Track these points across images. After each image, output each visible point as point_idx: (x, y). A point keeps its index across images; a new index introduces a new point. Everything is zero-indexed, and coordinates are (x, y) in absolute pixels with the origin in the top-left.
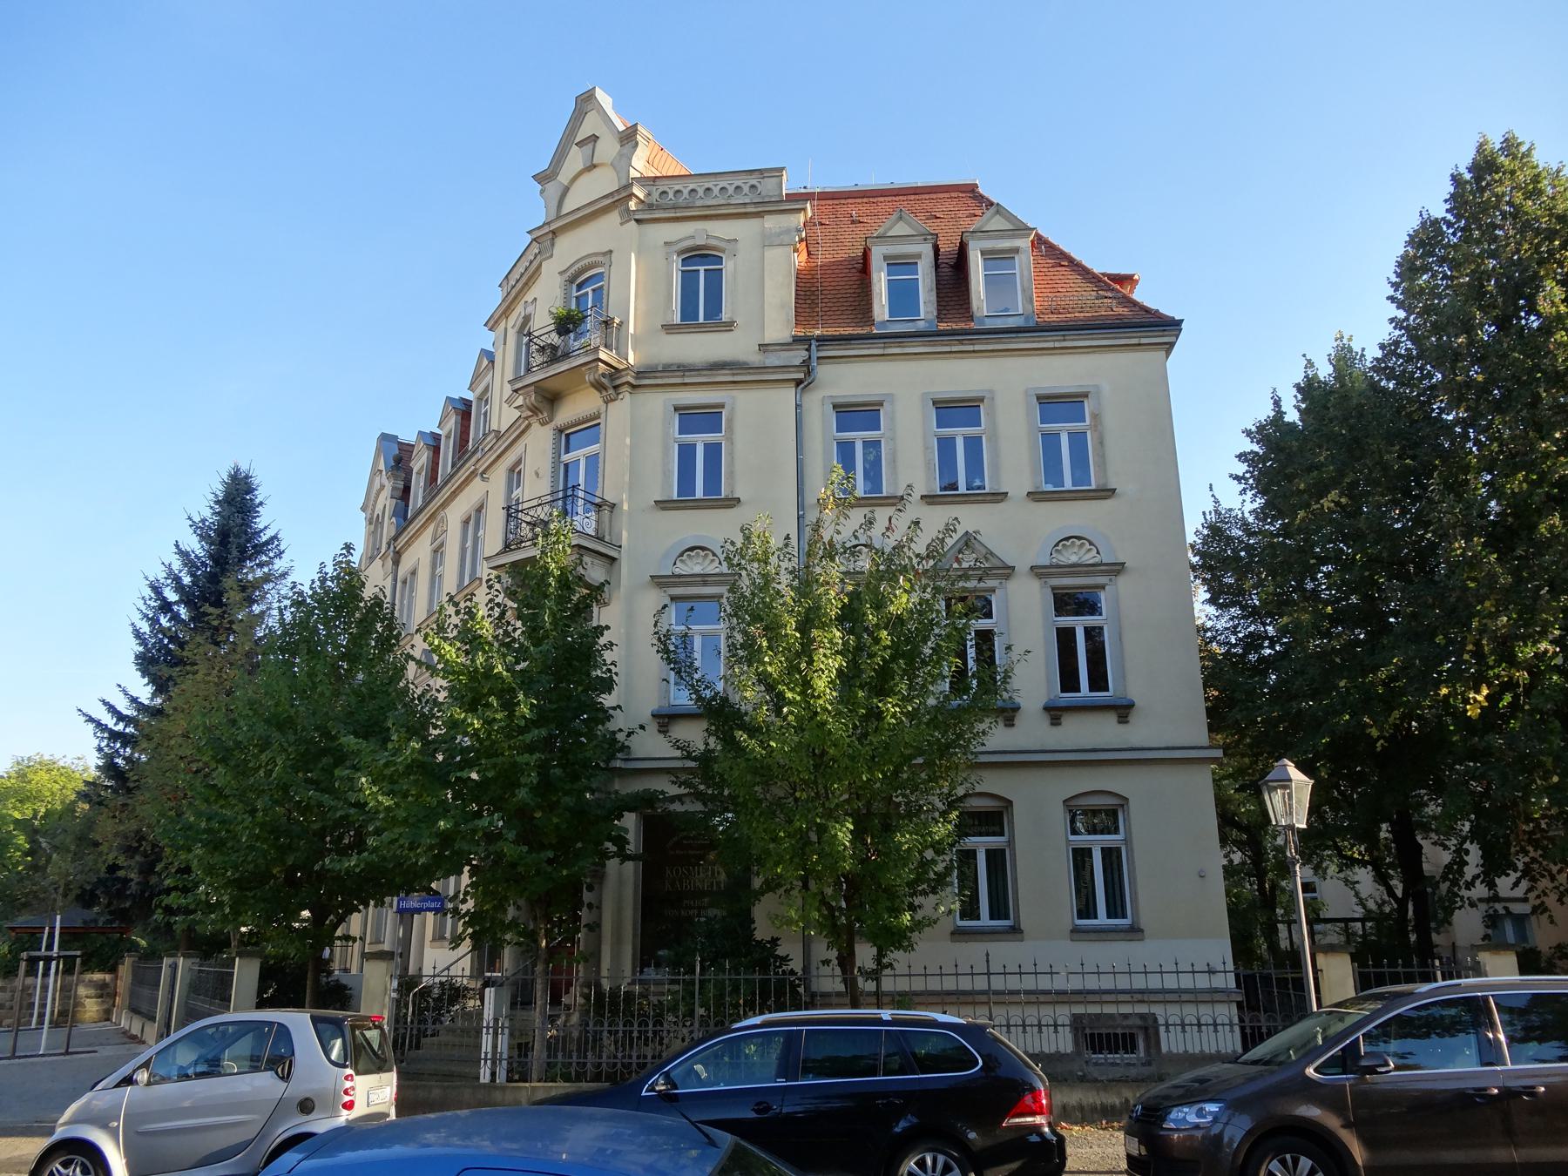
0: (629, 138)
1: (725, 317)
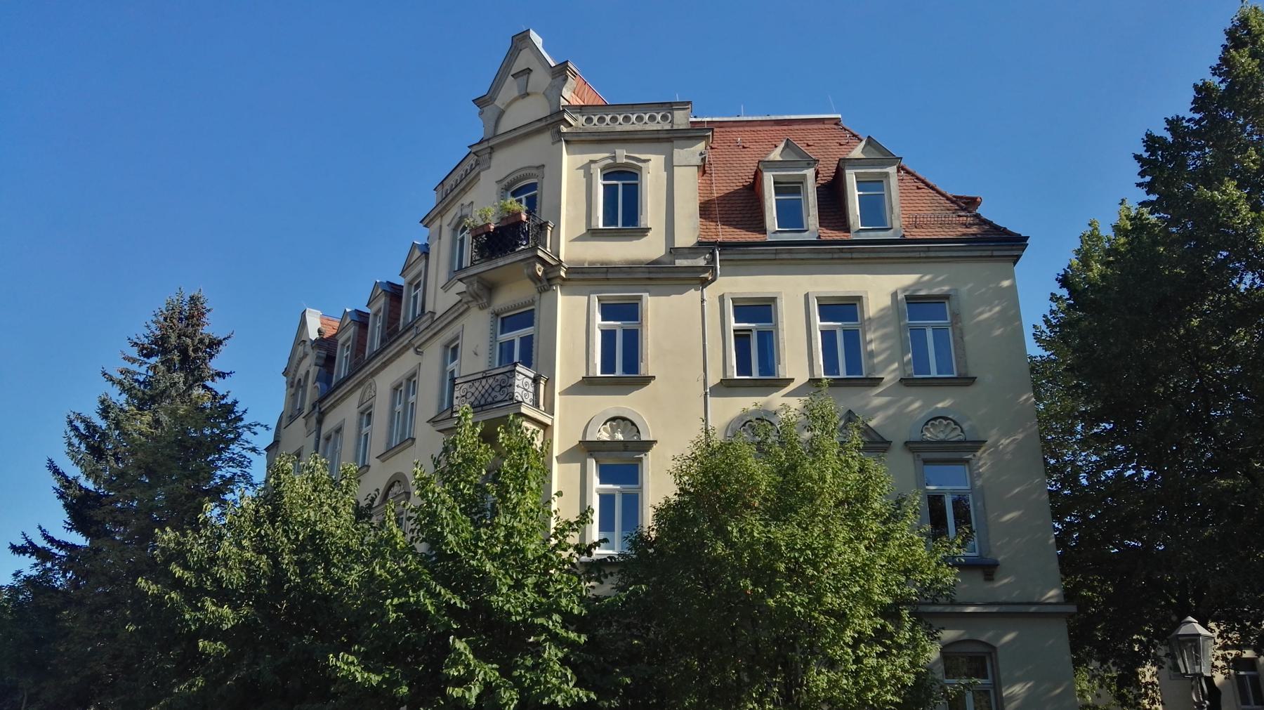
0: (561, 72)
1: (642, 224)
